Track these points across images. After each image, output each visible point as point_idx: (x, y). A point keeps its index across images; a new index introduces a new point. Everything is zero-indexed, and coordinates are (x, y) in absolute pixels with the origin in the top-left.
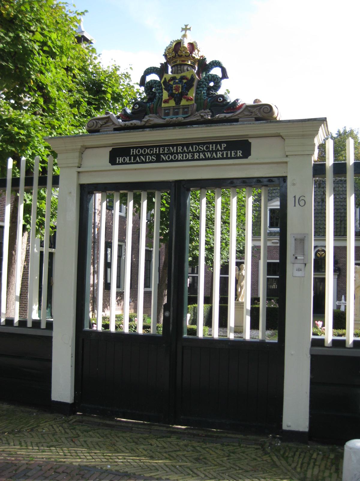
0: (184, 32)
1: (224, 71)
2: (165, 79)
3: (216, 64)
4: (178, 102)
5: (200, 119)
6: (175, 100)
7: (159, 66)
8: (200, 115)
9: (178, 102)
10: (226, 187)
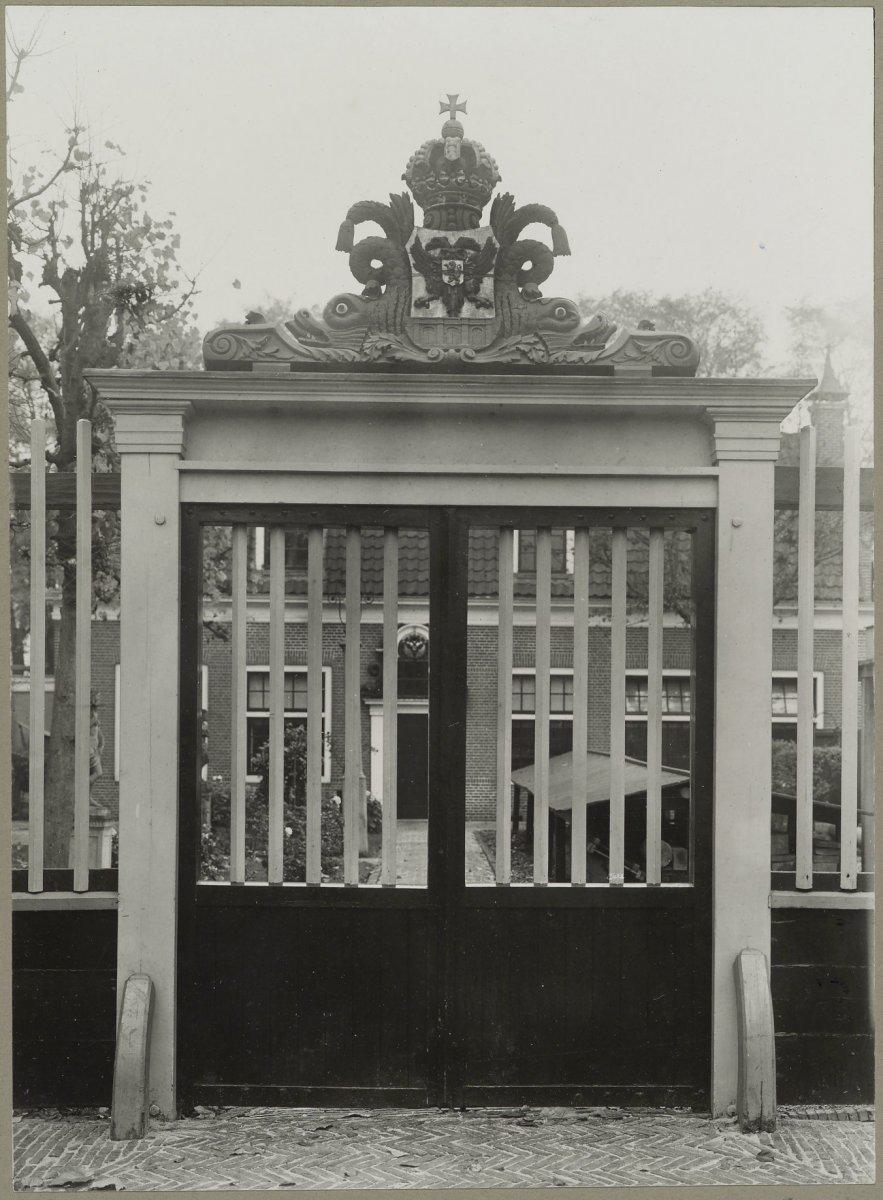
0: (447, 115)
1: (559, 236)
2: (417, 239)
3: (536, 214)
4: (453, 310)
5: (518, 360)
6: (446, 303)
7: (387, 202)
8: (518, 349)
9: (453, 310)
10: (325, 365)
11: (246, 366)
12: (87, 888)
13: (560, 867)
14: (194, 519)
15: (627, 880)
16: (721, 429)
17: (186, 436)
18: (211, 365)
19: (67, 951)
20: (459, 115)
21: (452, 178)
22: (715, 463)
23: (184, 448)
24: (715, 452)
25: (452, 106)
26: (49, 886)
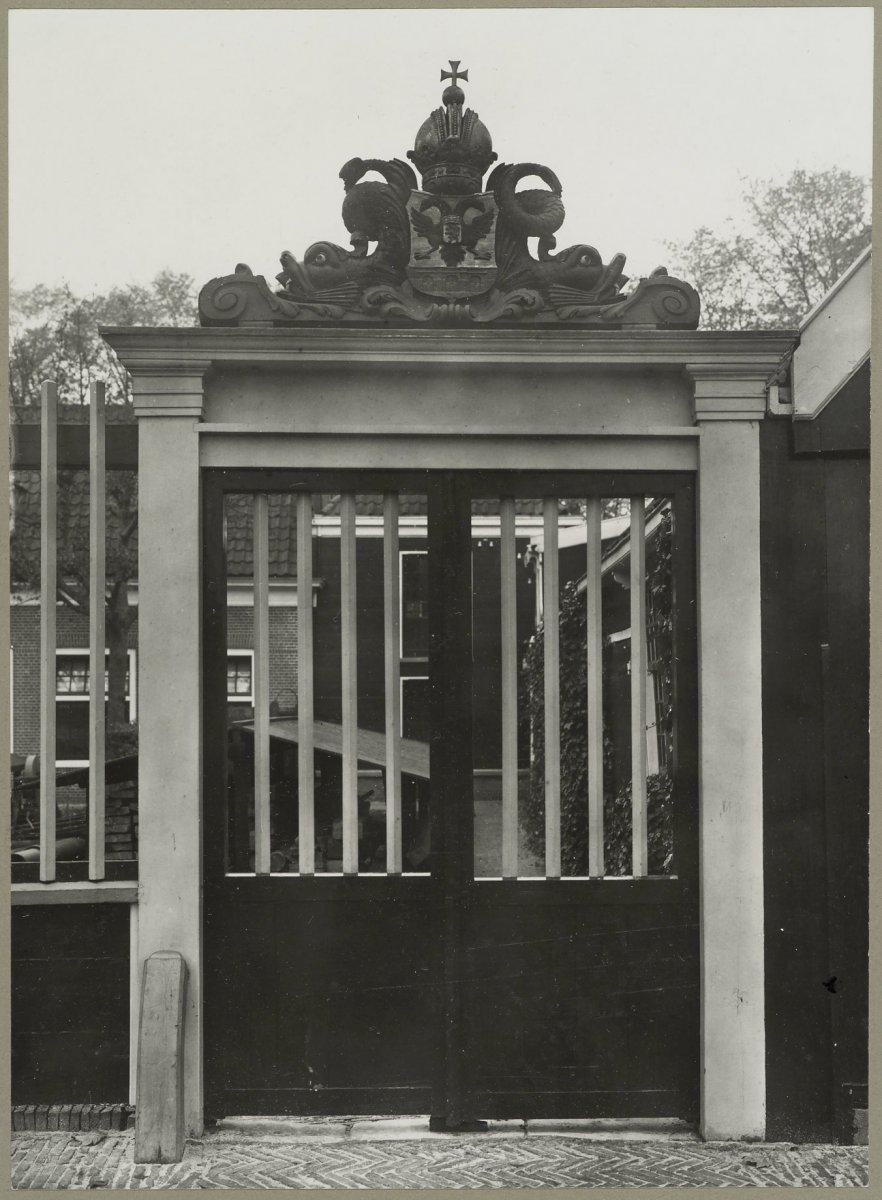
0: (448, 82)
11: (234, 322)
12: (102, 876)
13: (575, 857)
14: (219, 489)
15: (317, 869)
16: (702, 388)
17: (206, 398)
18: (205, 320)
19: (72, 954)
20: (460, 82)
21: (454, 142)
22: (696, 423)
23: (203, 410)
24: (696, 413)
25: (455, 73)
26: (63, 874)
